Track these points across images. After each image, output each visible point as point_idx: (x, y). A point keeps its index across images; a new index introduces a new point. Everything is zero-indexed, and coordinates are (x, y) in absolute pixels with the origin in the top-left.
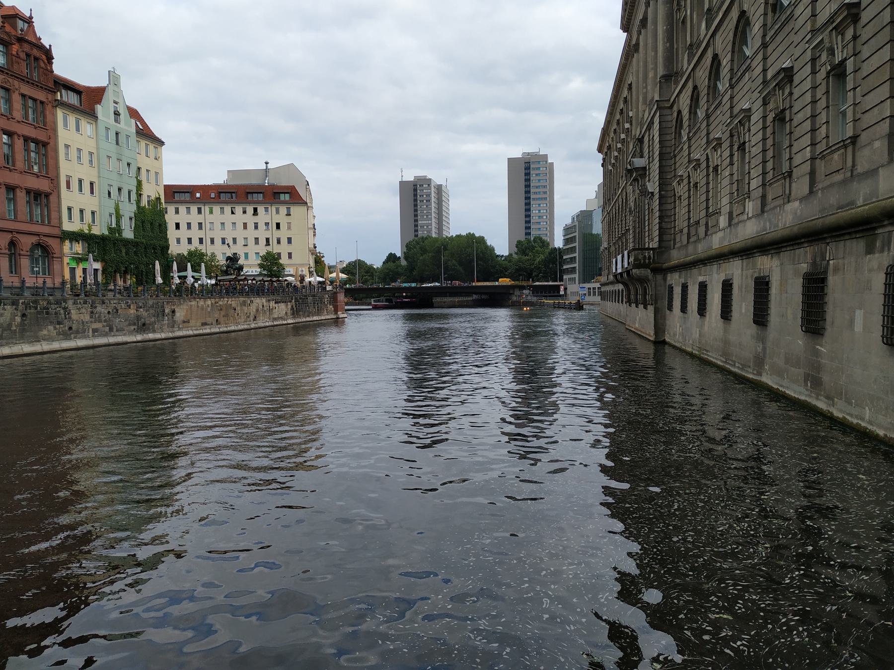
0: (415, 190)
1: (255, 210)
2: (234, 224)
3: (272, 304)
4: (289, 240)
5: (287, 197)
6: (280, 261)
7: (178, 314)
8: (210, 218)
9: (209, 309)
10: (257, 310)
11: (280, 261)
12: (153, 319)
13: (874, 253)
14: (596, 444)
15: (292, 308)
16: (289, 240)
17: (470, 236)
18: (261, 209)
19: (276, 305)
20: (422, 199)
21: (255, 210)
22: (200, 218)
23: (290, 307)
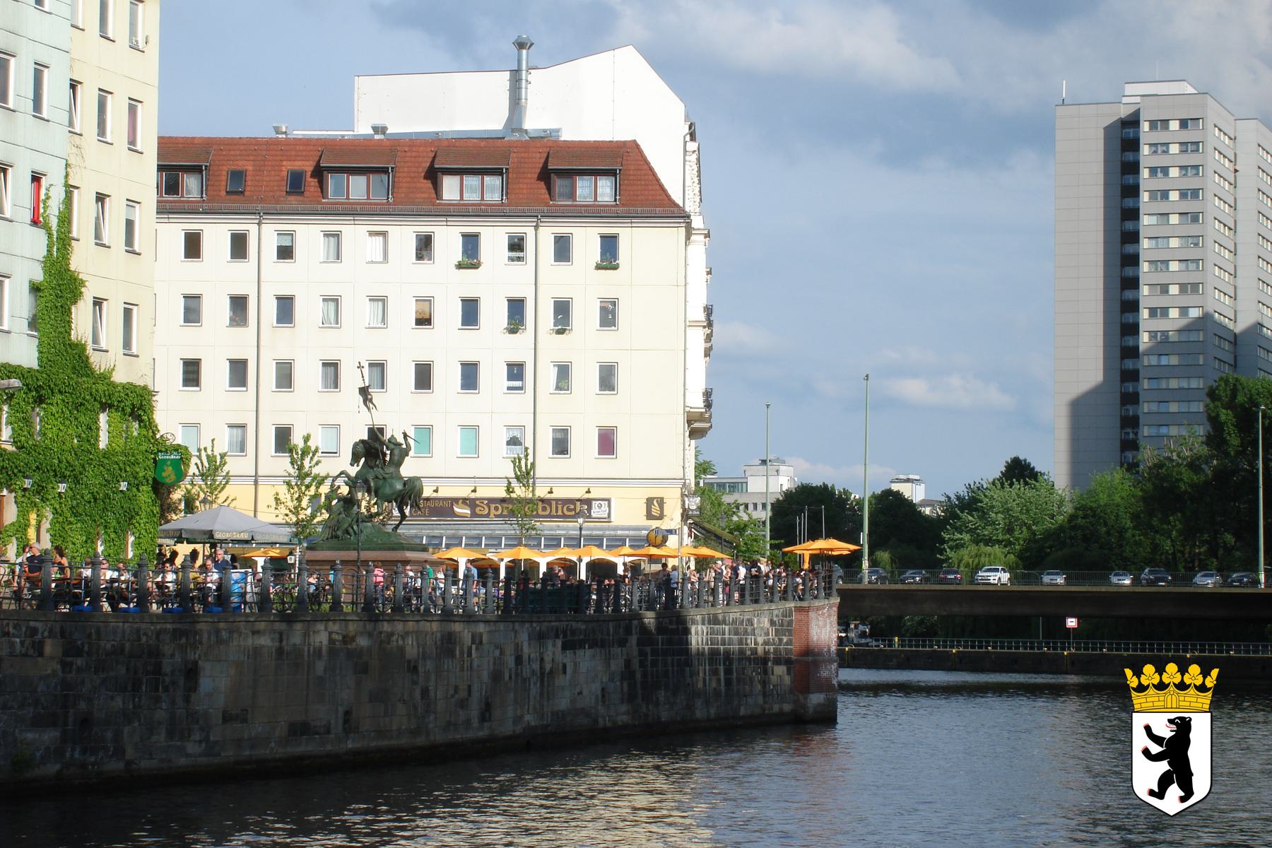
0: (1132, 145)
1: (471, 244)
2: (424, 321)
3: (553, 651)
4: (608, 379)
5: (605, 189)
6: (366, 438)
7: (205, 684)
8: (280, 278)
9: (320, 667)
10: (496, 676)
11: (366, 438)
12: (118, 702)
13: (874, 496)
14: (277, 130)
15: (628, 674)
16: (608, 379)
17: (825, 488)
18: (494, 237)
19: (568, 658)
20: (1159, 183)
21: (471, 244)
22: (240, 278)
23: (617, 665)
